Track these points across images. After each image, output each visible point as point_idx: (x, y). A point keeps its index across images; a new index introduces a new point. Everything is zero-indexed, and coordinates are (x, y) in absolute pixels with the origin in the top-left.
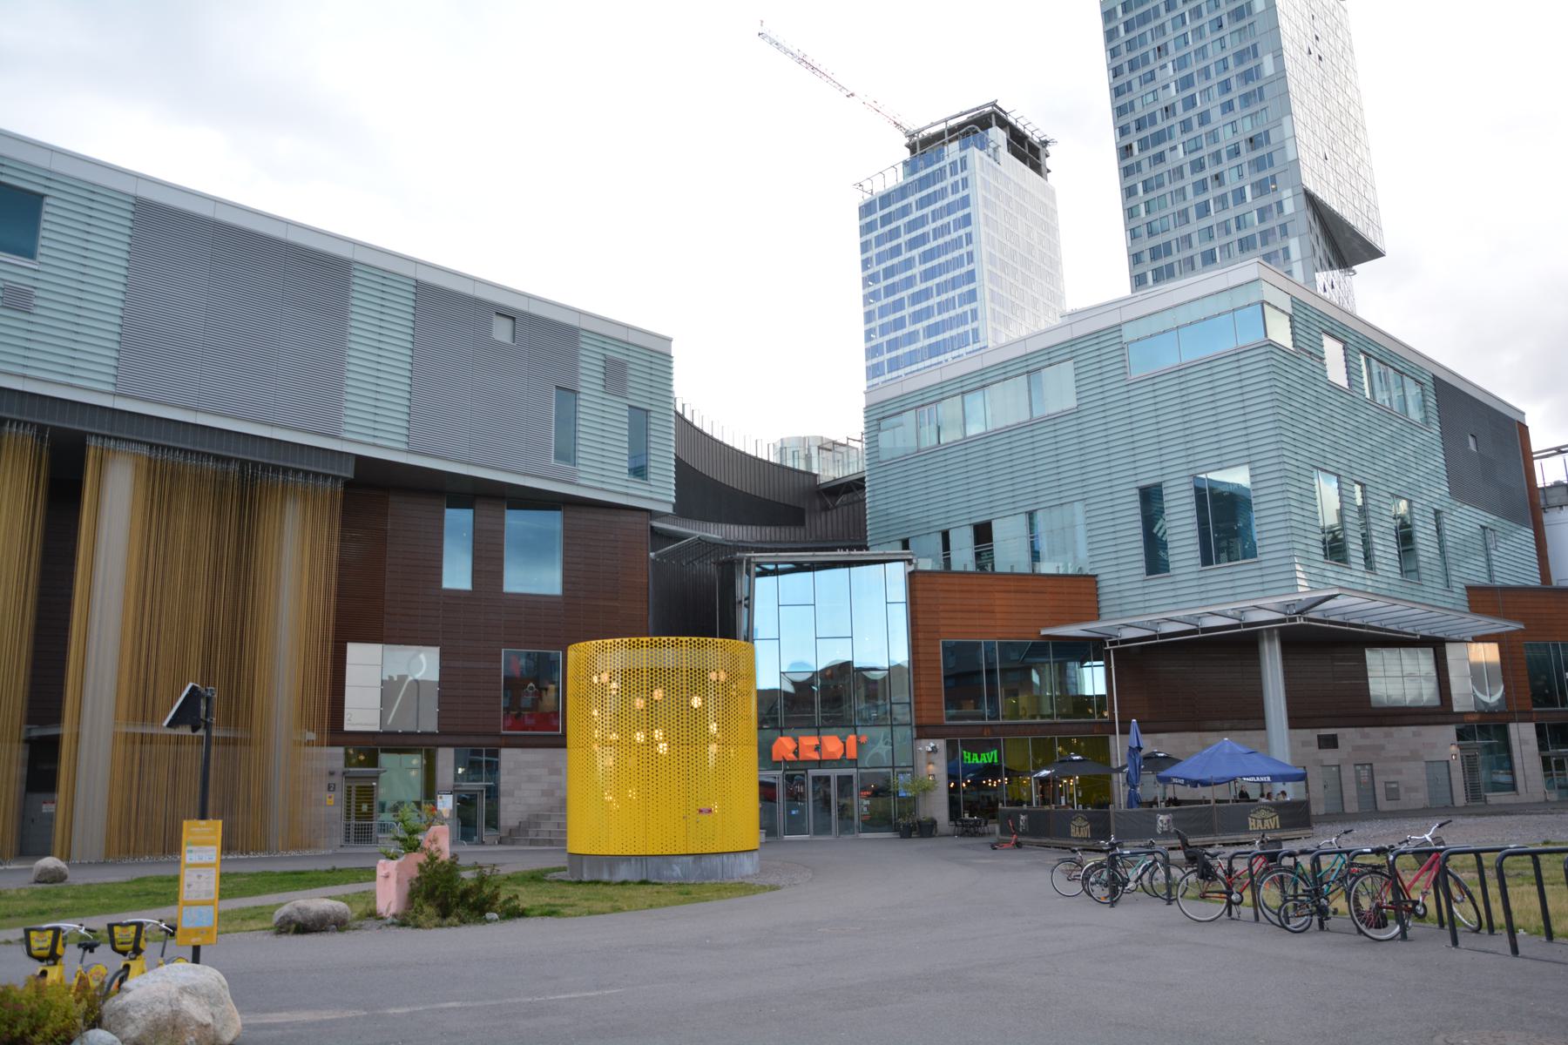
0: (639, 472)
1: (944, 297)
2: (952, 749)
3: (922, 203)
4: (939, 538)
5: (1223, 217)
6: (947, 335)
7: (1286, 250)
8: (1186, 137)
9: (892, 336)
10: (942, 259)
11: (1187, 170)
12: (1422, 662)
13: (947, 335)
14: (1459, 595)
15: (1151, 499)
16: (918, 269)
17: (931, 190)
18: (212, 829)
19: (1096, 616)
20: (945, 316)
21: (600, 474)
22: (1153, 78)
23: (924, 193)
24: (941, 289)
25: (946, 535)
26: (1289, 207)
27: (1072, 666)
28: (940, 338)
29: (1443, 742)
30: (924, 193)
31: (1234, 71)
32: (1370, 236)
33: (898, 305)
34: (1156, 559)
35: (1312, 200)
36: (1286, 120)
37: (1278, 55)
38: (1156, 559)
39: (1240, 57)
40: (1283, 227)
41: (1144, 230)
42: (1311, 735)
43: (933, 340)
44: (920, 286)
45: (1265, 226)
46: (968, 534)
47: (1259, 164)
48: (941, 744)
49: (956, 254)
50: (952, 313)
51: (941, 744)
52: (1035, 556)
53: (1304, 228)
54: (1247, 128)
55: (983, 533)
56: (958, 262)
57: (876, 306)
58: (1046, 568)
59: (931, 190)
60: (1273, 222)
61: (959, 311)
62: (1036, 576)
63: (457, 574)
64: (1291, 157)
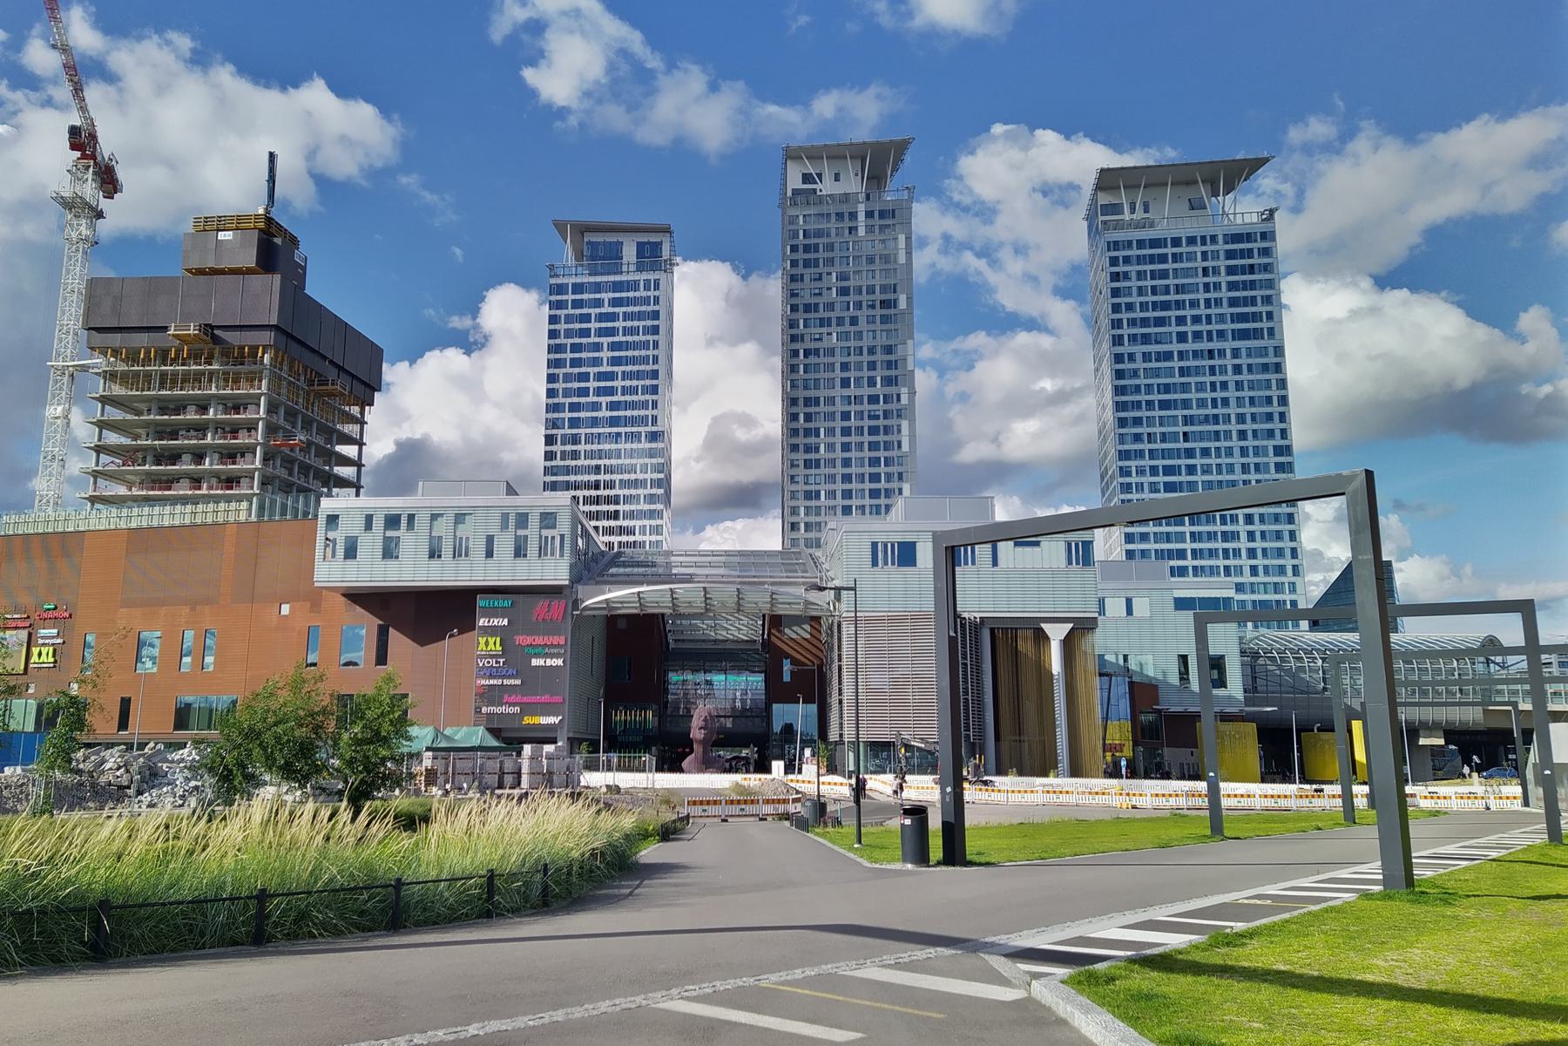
3: (616, 302)
8: (840, 329)
10: (630, 353)
11: (838, 352)
12: (1515, 620)
17: (624, 295)
18: (781, 763)
22: (820, 279)
23: (617, 295)
27: (1369, 129)
30: (617, 295)
39: (884, 289)
41: (800, 383)
43: (598, 296)
47: (890, 365)
49: (642, 413)
54: (882, 340)
56: (645, 360)
59: (624, 295)
60: (893, 406)
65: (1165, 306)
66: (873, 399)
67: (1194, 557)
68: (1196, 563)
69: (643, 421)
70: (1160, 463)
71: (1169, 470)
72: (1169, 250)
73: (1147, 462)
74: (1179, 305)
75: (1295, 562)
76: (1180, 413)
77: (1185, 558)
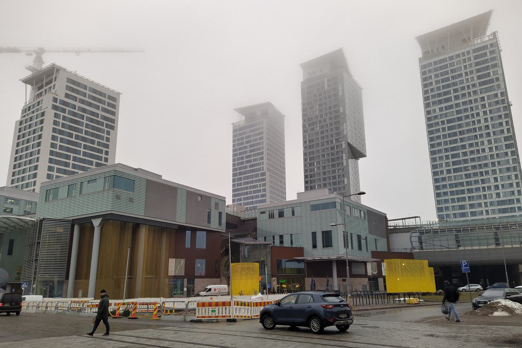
0: (220, 224)
1: (255, 158)
2: (277, 279)
3: (250, 132)
4: (272, 237)
5: (328, 146)
6: (255, 168)
7: (342, 157)
9: (240, 166)
13: (255, 168)
14: (370, 253)
15: (314, 234)
16: (248, 149)
19: (303, 256)
20: (255, 163)
21: (214, 226)
22: (314, 130)
24: (254, 155)
25: (274, 237)
26: (344, 146)
28: (253, 168)
29: (365, 281)
31: (334, 126)
32: (363, 152)
33: (242, 158)
34: (315, 246)
35: (349, 145)
36: (345, 124)
37: (344, 108)
38: (315, 246)
40: (342, 151)
42: (341, 279)
43: (251, 169)
44: (248, 154)
45: (338, 150)
46: (279, 237)
48: (276, 278)
50: (257, 162)
51: (276, 278)
52: (292, 243)
53: (347, 151)
55: (281, 237)
57: (236, 157)
58: (294, 246)
61: (259, 162)
62: (292, 248)
63: (188, 245)
64: (345, 134)
65: (448, 86)
66: (332, 148)
67: (469, 200)
68: (469, 195)
69: (259, 170)
70: (456, 197)
71: (453, 156)
72: (465, 188)
73: (447, 183)
74: (455, 84)
75: (519, 189)
76: (463, 173)
77: (464, 193)
